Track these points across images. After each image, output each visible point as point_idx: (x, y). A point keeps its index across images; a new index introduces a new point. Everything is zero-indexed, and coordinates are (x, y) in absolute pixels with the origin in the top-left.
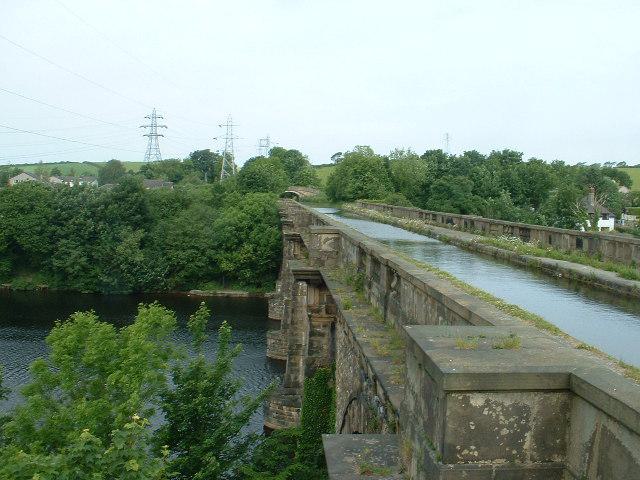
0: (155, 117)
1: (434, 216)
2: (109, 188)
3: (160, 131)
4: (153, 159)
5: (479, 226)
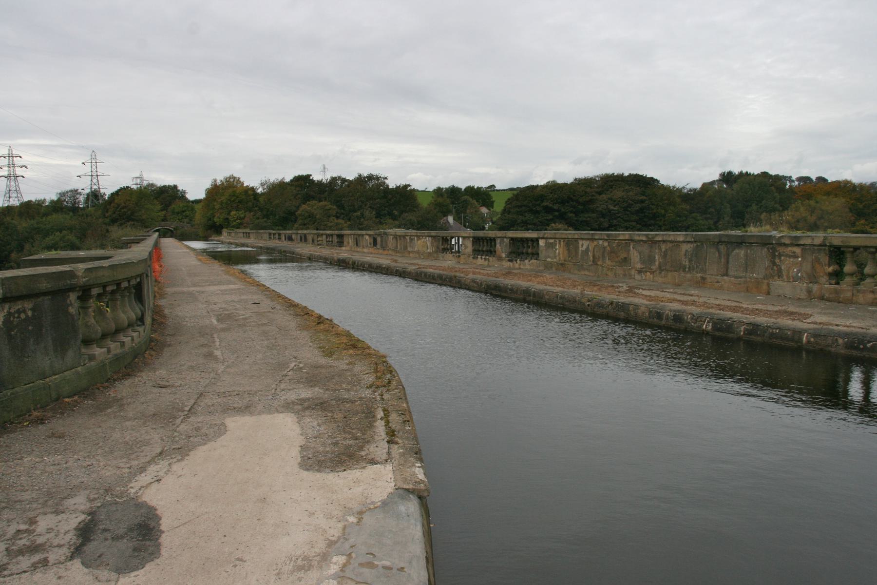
0: (11, 156)
3: (19, 171)
4: (15, 202)
5: (310, 238)
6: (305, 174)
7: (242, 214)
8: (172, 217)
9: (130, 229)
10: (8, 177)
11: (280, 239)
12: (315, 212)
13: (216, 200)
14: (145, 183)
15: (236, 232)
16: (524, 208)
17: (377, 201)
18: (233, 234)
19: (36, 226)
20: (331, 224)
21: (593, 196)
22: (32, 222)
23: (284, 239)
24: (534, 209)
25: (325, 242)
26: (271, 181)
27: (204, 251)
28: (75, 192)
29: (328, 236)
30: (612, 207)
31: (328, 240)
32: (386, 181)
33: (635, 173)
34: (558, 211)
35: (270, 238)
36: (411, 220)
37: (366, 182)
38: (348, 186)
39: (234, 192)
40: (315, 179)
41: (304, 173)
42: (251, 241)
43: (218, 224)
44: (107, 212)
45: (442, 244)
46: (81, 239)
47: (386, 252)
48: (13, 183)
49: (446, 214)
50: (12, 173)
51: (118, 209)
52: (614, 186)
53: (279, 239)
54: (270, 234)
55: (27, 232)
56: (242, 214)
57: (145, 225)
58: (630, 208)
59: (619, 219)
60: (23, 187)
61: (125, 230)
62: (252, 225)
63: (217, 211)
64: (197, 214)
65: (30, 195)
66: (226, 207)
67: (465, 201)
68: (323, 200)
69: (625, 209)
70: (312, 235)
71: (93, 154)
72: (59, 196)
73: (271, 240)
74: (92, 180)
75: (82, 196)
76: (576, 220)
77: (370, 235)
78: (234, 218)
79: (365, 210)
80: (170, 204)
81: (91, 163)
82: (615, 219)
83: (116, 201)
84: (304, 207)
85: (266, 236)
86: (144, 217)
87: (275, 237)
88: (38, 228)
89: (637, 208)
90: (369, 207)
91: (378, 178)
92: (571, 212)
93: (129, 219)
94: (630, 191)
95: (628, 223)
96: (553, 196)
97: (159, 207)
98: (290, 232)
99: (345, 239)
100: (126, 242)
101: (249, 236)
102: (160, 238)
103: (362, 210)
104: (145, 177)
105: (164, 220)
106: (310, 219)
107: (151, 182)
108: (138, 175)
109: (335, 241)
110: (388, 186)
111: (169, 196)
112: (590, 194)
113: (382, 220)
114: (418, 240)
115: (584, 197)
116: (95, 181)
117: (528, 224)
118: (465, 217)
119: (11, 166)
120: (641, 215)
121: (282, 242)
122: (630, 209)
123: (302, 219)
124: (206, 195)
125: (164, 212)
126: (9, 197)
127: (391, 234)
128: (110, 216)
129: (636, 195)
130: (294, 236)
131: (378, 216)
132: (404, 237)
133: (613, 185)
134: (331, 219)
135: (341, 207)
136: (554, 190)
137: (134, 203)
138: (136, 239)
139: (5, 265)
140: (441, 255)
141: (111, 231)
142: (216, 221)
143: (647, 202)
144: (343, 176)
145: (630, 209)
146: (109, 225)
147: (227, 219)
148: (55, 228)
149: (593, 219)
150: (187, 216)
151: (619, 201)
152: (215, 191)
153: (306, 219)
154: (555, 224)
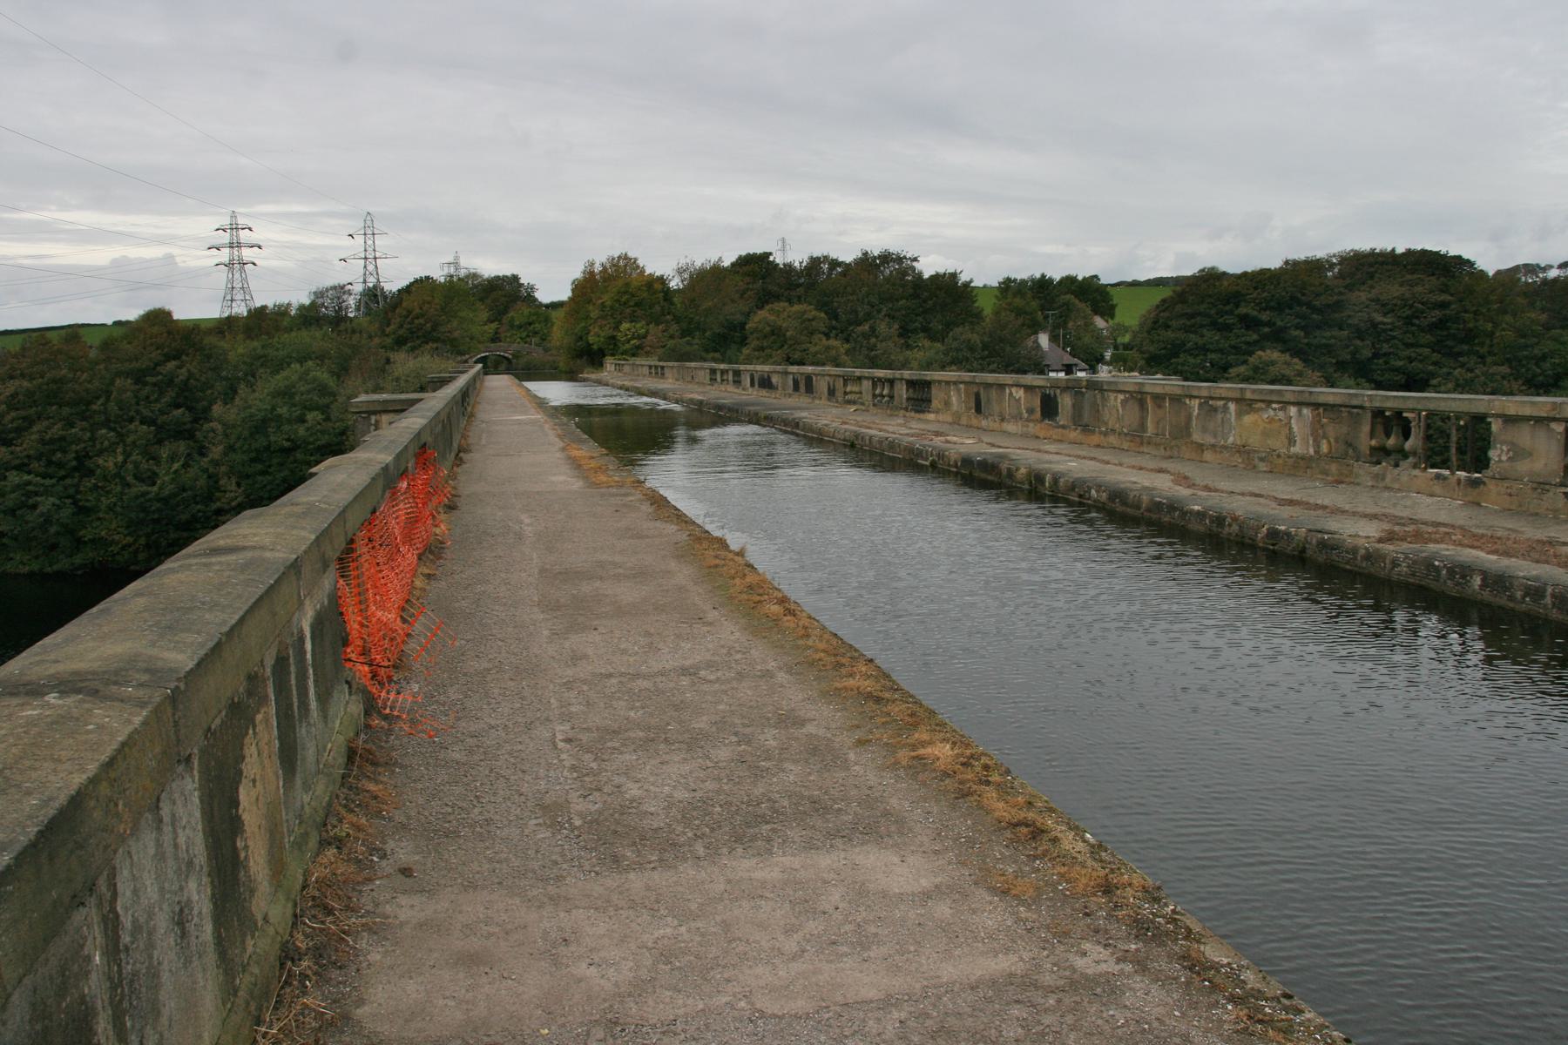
0: (235, 228)
1: (737, 373)
2: (42, 519)
3: (247, 254)
4: (241, 310)
5: (822, 385)
6: (759, 250)
7: (642, 328)
8: (509, 335)
9: (429, 357)
10: (230, 265)
11: (737, 382)
12: (784, 325)
13: (591, 300)
14: (462, 273)
15: (633, 364)
16: (1198, 319)
17: (901, 303)
18: (627, 369)
19: (260, 351)
20: (817, 348)
21: (1341, 293)
22: (255, 344)
23: (749, 385)
24: (1220, 320)
25: (867, 397)
26: (698, 264)
27: (575, 411)
28: (341, 290)
29: (876, 382)
30: (1379, 318)
31: (877, 392)
32: (915, 264)
33: (1419, 248)
34: (1269, 324)
35: (713, 380)
36: (969, 340)
37: (878, 266)
38: (844, 274)
39: (627, 285)
40: (777, 261)
41: (758, 249)
42: (668, 384)
43: (595, 347)
44: (388, 325)
45: (1372, 435)
46: (339, 377)
47: (1096, 439)
48: (237, 275)
49: (1035, 328)
50: (236, 258)
51: (409, 320)
52: (1377, 275)
53: (734, 382)
54: (713, 371)
55: (244, 363)
56: (642, 328)
57: (457, 349)
58: (1417, 318)
59: (1396, 341)
60: (253, 285)
61: (420, 359)
62: (663, 350)
63: (594, 323)
64: (555, 328)
65: (266, 296)
66: (612, 315)
67: (1067, 304)
68: (795, 300)
69: (1408, 321)
70: (827, 378)
71: (369, 218)
72: (312, 297)
73: (716, 385)
74: (365, 267)
75: (352, 297)
76: (1307, 344)
77: (1029, 388)
78: (626, 335)
79: (878, 321)
80: (505, 311)
81: (365, 234)
82: (1387, 341)
83: (404, 304)
84: (763, 314)
85: (703, 376)
86: (456, 334)
87: (725, 377)
88: (265, 356)
89: (1434, 319)
90: (885, 315)
91: (900, 259)
92: (1297, 328)
93: (428, 338)
94: (1417, 284)
95: (1412, 350)
96: (1259, 294)
97: (485, 315)
98: (767, 368)
99: (937, 395)
100: (364, 409)
101: (663, 374)
102: (486, 374)
103: (871, 322)
104: (463, 262)
105: (495, 339)
106: (773, 337)
107: (472, 271)
108: (451, 259)
109: (901, 396)
110: (920, 273)
111: (505, 296)
112: (1336, 290)
113: (910, 342)
114: (1239, 414)
115: (1322, 298)
116: (371, 268)
117: (1208, 350)
118: (1064, 336)
119: (235, 245)
120: (1439, 332)
121: (744, 389)
122: (1417, 322)
123: (758, 339)
124: (573, 290)
125: (494, 326)
126: (232, 301)
127: (1122, 388)
128: (394, 333)
129: (1430, 293)
130: (775, 379)
131: (905, 332)
132: (1177, 400)
133: (1376, 272)
134: (817, 337)
135: (833, 315)
136: (1260, 281)
137: (438, 307)
138: (394, 401)
139: (202, 425)
140: (1364, 471)
141: (394, 363)
142: (591, 342)
143: (1453, 306)
144: (833, 255)
145: (1417, 322)
146: (392, 349)
147: (614, 338)
148: (294, 355)
149: (1341, 341)
150: (536, 333)
151: (1396, 305)
152: (587, 287)
153: (765, 337)
154: (1264, 351)
